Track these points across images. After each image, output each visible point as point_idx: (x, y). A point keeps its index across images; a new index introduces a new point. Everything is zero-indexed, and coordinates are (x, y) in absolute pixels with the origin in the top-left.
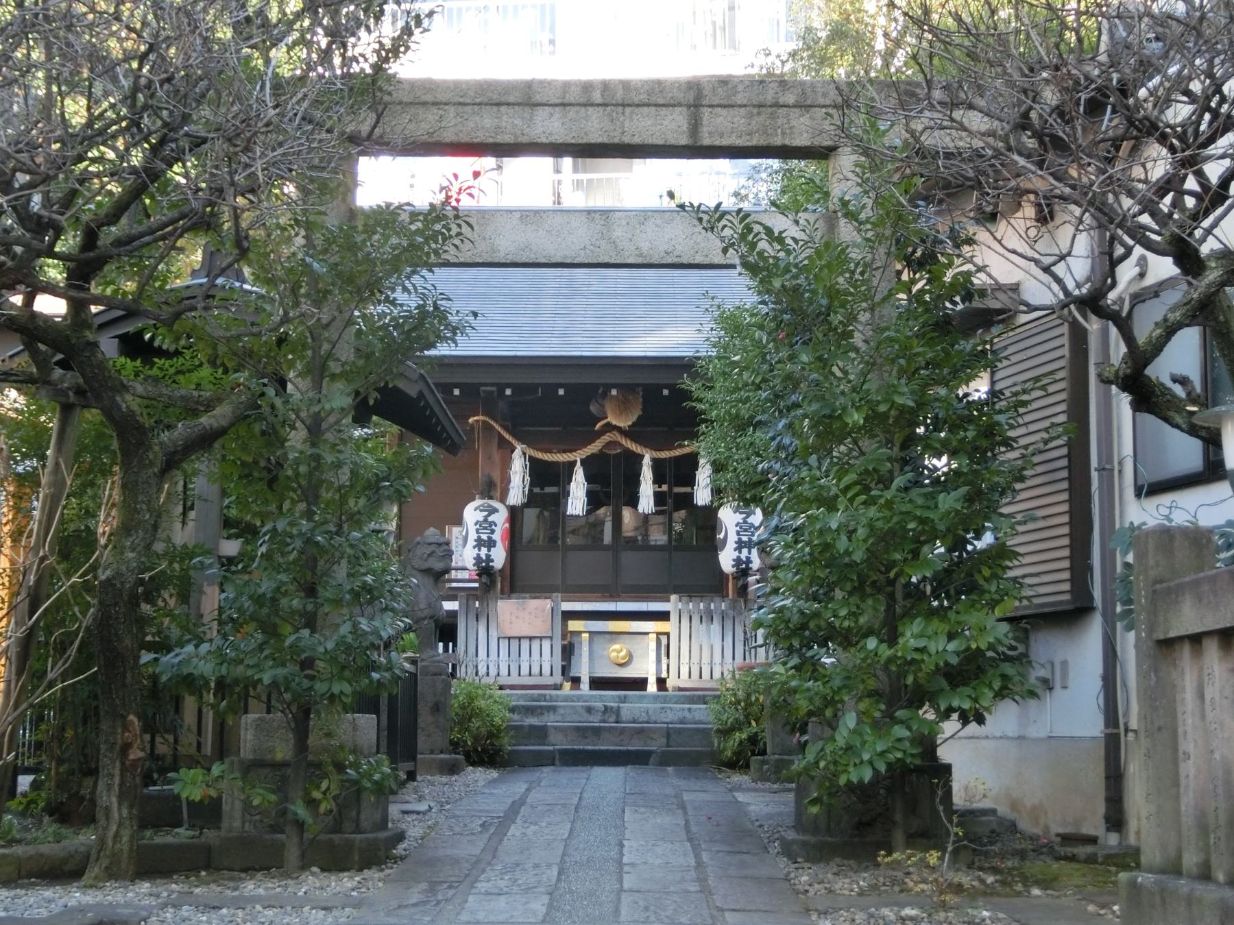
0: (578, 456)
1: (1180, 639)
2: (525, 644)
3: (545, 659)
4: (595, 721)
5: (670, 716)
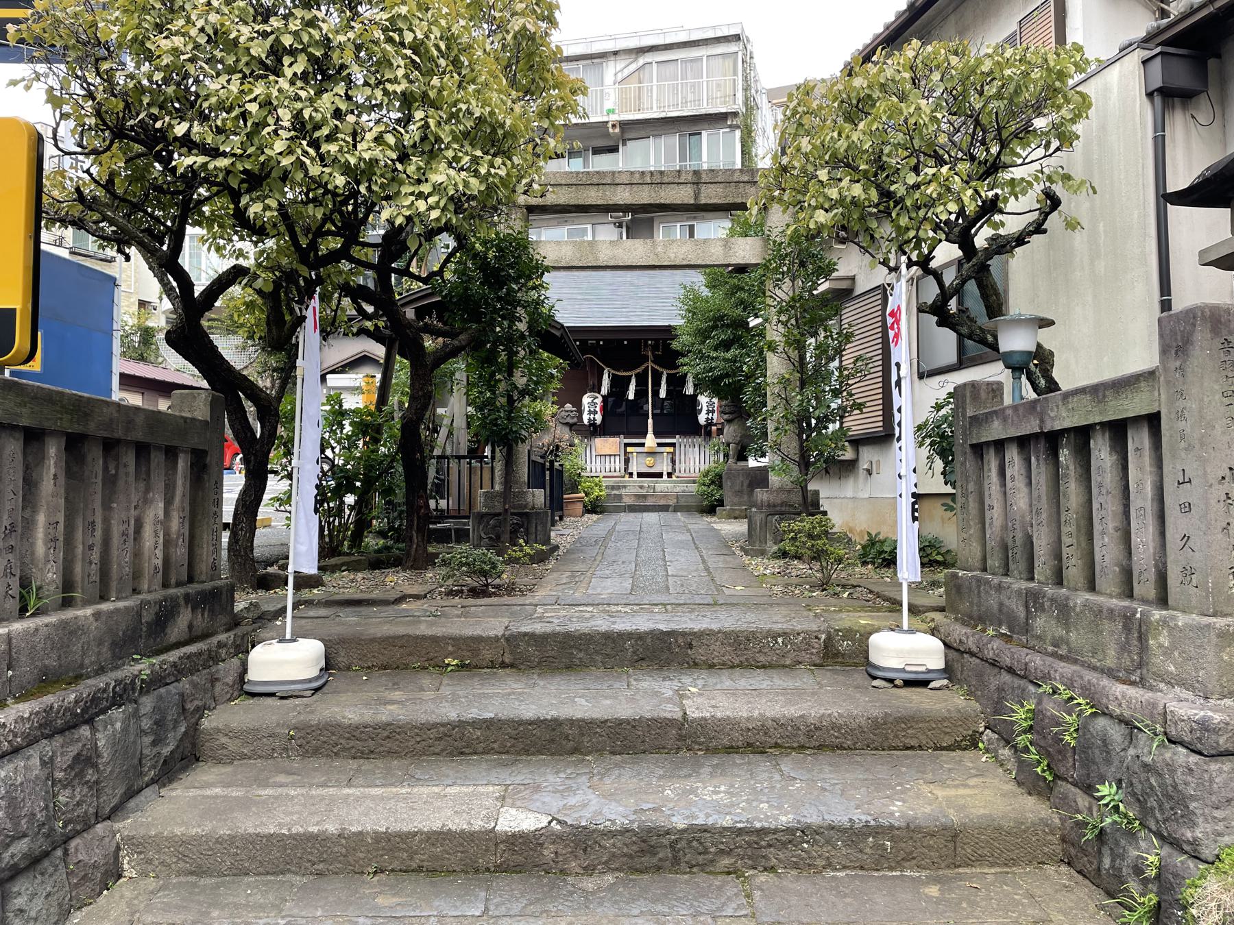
0: (633, 373)
1: (988, 443)
2: (1102, 453)
3: (618, 464)
4: (643, 492)
5: (678, 489)
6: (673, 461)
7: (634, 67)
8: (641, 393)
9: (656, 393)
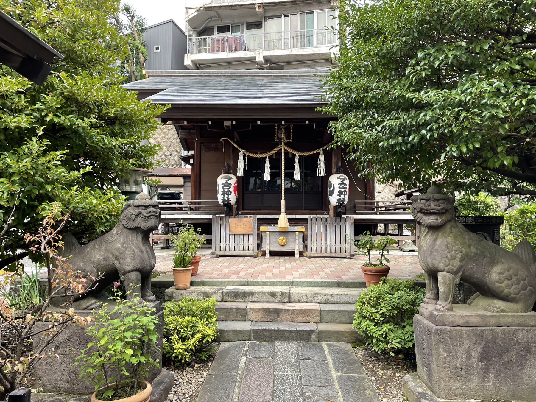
0: (267, 155)
3: (252, 242)
6: (305, 239)
8: (275, 175)
9: (290, 175)
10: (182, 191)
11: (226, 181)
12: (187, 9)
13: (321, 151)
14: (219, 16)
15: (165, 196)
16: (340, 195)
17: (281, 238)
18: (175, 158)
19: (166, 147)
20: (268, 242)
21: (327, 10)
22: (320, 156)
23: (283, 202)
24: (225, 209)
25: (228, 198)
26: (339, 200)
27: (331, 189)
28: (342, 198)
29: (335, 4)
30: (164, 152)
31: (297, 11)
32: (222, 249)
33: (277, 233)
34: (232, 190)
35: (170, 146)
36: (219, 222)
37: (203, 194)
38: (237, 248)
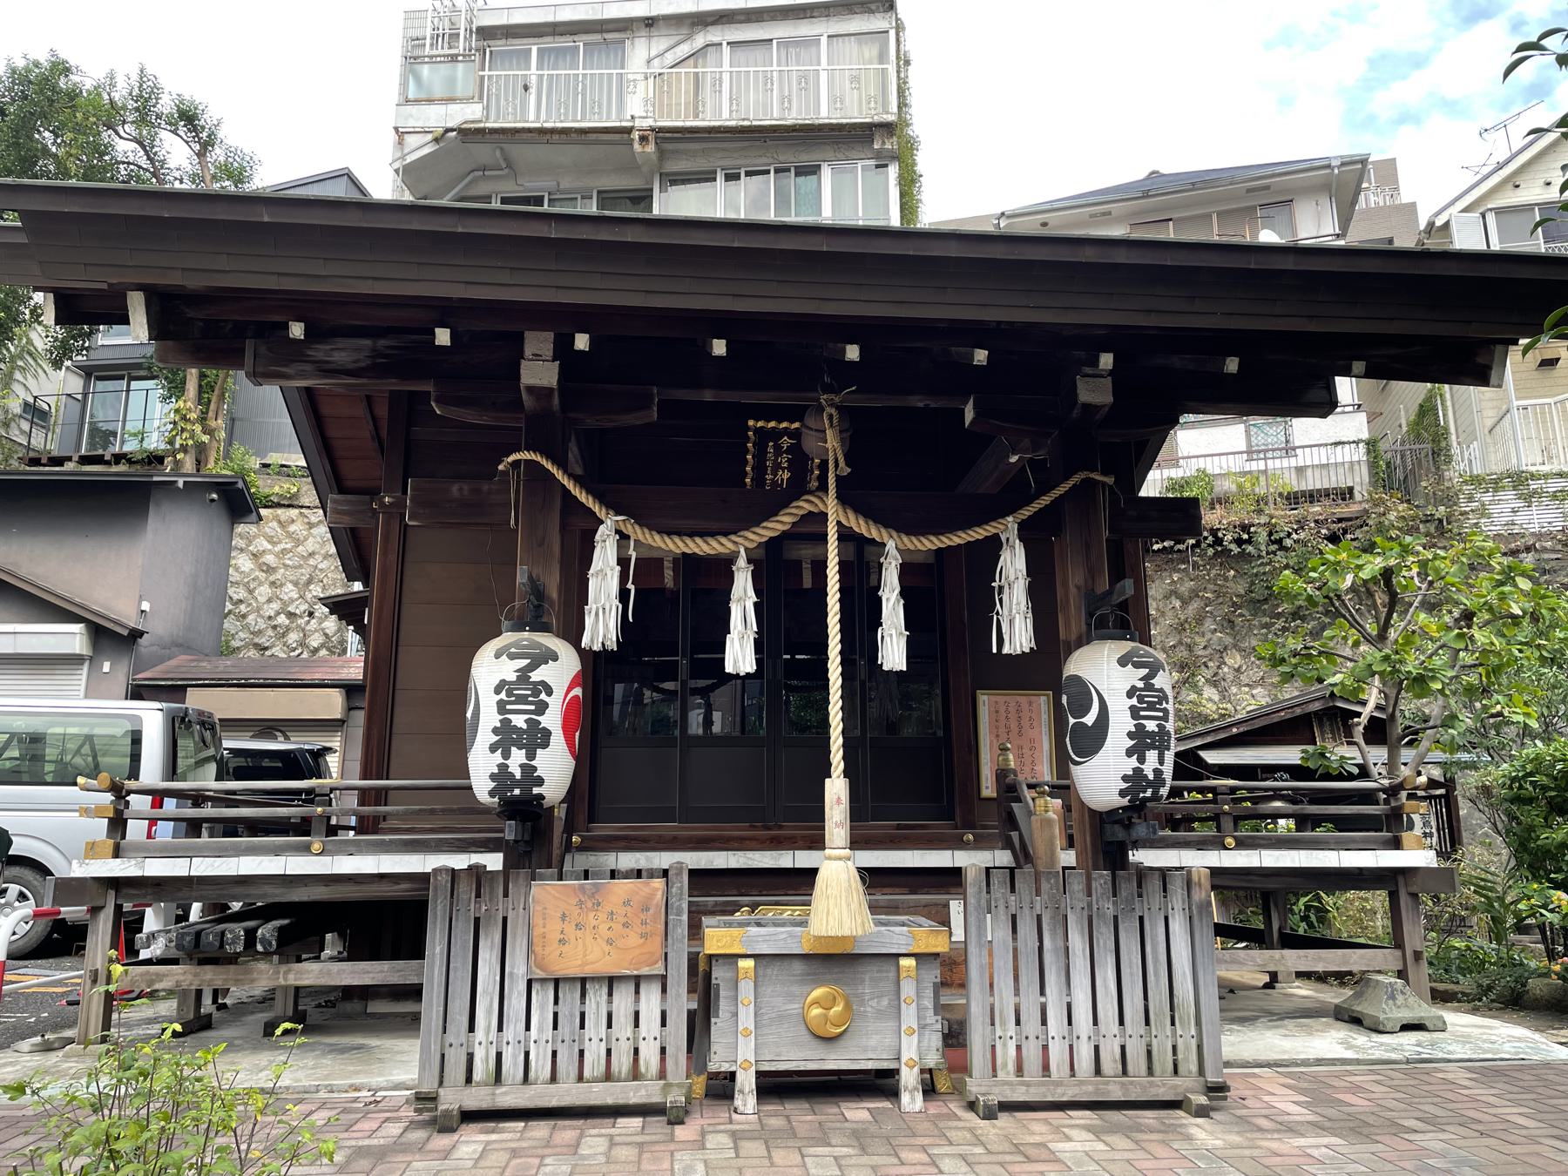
3: (649, 1024)
7: (684, 49)
10: (335, 742)
11: (523, 675)
12: (401, 134)
13: (1008, 528)
14: (509, 166)
15: (266, 763)
16: (1138, 751)
17: (819, 992)
18: (326, 624)
19: (296, 584)
20: (746, 1019)
21: (860, 164)
22: (1005, 556)
23: (836, 789)
24: (510, 830)
25: (528, 770)
26: (1136, 779)
27: (1089, 719)
28: (1149, 768)
29: (888, 146)
30: (285, 604)
31: (764, 160)
32: (478, 1075)
33: (798, 967)
34: (552, 720)
35: (309, 582)
36: (469, 907)
37: (401, 748)
38: (567, 1065)
